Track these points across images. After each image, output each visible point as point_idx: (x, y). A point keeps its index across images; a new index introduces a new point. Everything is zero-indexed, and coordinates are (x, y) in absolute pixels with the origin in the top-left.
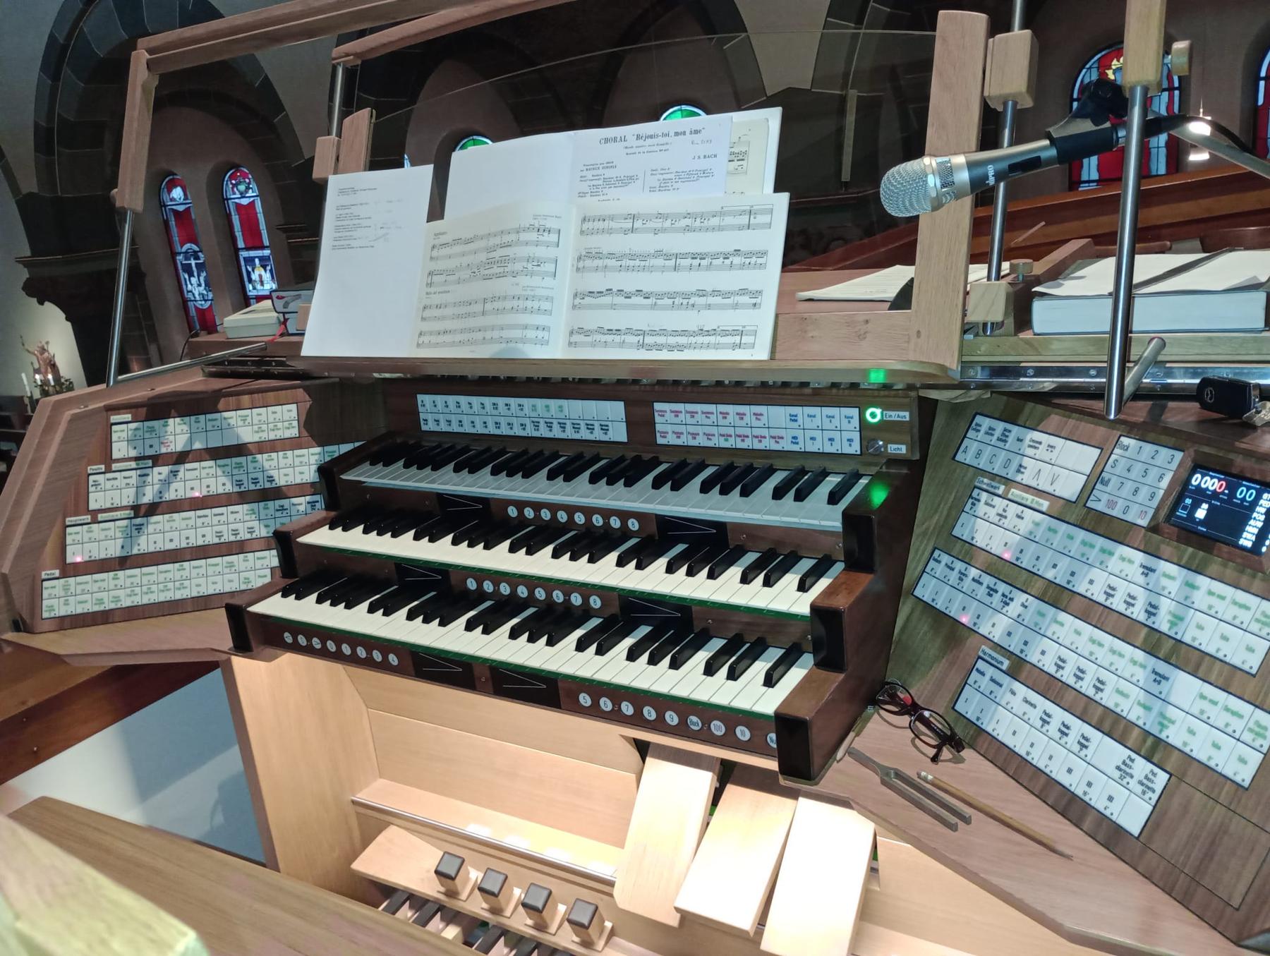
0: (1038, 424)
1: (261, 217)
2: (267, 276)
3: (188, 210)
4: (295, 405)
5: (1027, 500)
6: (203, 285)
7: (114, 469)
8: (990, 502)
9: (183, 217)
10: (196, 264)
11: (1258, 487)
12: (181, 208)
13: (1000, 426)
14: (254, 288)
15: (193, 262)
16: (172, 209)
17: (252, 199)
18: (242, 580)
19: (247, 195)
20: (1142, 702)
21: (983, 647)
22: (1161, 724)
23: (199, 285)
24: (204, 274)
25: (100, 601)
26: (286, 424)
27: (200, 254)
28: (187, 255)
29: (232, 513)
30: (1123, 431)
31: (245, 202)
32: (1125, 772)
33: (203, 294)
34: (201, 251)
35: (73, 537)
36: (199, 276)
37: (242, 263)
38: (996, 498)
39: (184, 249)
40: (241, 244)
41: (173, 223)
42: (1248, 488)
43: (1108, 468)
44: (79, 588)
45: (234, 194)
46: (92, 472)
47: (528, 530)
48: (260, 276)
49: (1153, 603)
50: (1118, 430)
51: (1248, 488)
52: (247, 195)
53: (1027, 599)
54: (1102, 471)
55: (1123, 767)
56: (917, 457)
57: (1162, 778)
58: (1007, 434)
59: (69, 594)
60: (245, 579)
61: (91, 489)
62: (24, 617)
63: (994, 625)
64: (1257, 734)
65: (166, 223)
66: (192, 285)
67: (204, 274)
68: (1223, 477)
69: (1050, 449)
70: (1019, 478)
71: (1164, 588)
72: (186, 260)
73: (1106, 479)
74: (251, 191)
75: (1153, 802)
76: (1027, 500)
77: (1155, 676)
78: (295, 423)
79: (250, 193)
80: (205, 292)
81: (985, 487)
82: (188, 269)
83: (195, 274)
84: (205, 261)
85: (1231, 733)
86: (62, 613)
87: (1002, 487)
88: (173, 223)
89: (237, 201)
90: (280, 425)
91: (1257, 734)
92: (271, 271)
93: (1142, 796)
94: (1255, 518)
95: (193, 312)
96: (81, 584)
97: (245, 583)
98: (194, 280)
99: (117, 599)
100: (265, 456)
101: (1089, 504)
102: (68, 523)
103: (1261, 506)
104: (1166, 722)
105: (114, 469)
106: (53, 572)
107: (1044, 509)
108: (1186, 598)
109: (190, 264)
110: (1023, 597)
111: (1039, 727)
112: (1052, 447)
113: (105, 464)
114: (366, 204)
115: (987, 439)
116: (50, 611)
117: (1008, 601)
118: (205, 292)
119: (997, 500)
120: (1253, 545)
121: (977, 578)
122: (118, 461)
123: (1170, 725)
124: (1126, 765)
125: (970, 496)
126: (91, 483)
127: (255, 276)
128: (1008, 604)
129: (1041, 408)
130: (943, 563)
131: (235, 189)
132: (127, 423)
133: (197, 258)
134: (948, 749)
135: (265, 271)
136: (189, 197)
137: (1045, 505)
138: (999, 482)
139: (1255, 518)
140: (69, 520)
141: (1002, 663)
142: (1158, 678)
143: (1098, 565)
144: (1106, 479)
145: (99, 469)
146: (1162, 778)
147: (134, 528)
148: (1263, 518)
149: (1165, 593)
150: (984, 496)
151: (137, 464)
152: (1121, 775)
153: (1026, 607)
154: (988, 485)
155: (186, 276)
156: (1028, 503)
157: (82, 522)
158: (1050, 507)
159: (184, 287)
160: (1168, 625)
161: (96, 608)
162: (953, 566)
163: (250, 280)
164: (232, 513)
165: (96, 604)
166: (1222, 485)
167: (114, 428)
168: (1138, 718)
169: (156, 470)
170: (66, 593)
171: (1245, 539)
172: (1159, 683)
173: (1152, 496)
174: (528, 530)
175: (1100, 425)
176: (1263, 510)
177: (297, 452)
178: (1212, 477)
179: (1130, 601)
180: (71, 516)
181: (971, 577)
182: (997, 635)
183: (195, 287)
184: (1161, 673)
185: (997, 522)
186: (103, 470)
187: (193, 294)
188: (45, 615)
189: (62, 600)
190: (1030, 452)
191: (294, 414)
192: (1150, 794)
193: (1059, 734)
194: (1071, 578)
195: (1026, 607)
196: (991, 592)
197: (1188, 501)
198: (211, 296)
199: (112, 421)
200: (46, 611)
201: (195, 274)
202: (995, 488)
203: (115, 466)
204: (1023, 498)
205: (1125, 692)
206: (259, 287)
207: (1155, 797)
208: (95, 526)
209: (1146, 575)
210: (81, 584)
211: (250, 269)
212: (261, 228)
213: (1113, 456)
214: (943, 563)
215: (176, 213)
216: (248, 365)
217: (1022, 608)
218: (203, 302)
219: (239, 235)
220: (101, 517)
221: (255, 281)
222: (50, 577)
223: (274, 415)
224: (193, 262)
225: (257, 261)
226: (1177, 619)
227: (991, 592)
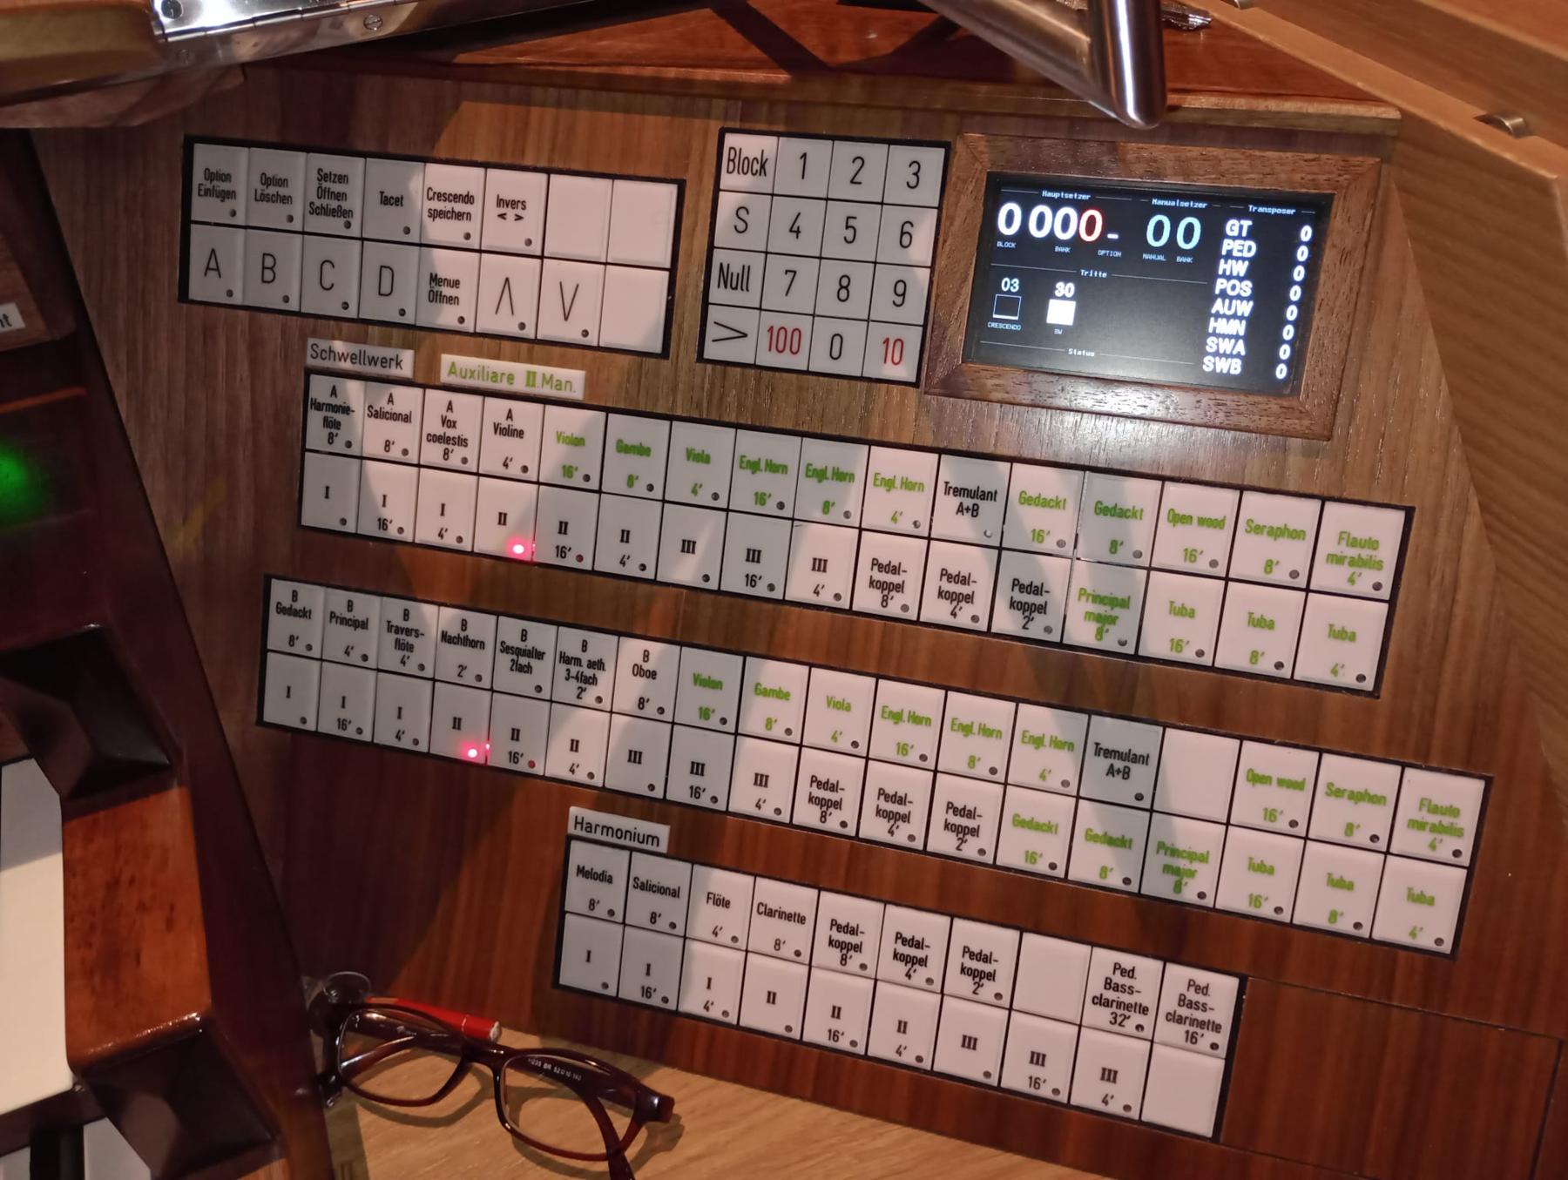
0: (433, 137)
5: (511, 378)
8: (383, 404)
11: (1202, 205)
13: (299, 169)
20: (1099, 831)
21: (574, 811)
22: (1176, 871)
30: (726, 118)
32: (1119, 1004)
38: (400, 392)
42: (1176, 216)
43: (723, 235)
47: (402, 1040)
49: (1025, 581)
50: (708, 115)
51: (1176, 216)
53: (646, 655)
54: (711, 247)
55: (1110, 995)
56: (69, 325)
57: (1222, 990)
58: (337, 188)
63: (574, 746)
64: (1436, 829)
68: (1085, 197)
69: (511, 213)
70: (447, 317)
71: (1039, 535)
73: (736, 269)
75: (1222, 1051)
76: (511, 378)
77: (1109, 761)
81: (346, 365)
85: (1287, 829)
87: (407, 356)
91: (1436, 829)
93: (1189, 1045)
94: (1223, 295)
101: (712, 351)
103: (1229, 255)
104: (1182, 863)
107: (578, 394)
108: (1114, 546)
110: (633, 649)
111: (836, 964)
112: (513, 204)
114: (220, 276)
115: (272, 214)
117: (589, 672)
119: (406, 399)
120: (1244, 367)
121: (454, 631)
123: (1195, 866)
124: (1116, 988)
125: (307, 403)
128: (593, 681)
129: (414, 89)
130: (318, 615)
134: (363, 1081)
137: (573, 380)
138: (386, 343)
139: (1223, 295)
141: (654, 839)
142: (1119, 764)
143: (817, 515)
144: (736, 269)
146: (1222, 990)
148: (1246, 288)
149: (1049, 545)
150: (354, 392)
152: (1115, 1016)
153: (652, 675)
154: (353, 358)
156: (519, 386)
158: (590, 384)
160: (1093, 627)
162: (358, 614)
166: (1092, 220)
168: (1104, 871)
171: (1217, 354)
172: (1126, 774)
173: (901, 293)
174: (402, 1040)
175: (643, 112)
176: (1241, 268)
178: (1055, 205)
179: (956, 588)
181: (433, 633)
182: (590, 766)
184: (1123, 749)
185: (441, 462)
190: (440, 231)
192: (1209, 1037)
193: (901, 968)
194: (563, 541)
195: (652, 675)
196: (523, 661)
197: (1010, 285)
202: (385, 362)
204: (559, 385)
205: (1042, 819)
207: (1222, 1039)
209: (974, 511)
213: (724, 197)
214: (318, 615)
217: (641, 682)
226: (1108, 606)
227: (523, 661)
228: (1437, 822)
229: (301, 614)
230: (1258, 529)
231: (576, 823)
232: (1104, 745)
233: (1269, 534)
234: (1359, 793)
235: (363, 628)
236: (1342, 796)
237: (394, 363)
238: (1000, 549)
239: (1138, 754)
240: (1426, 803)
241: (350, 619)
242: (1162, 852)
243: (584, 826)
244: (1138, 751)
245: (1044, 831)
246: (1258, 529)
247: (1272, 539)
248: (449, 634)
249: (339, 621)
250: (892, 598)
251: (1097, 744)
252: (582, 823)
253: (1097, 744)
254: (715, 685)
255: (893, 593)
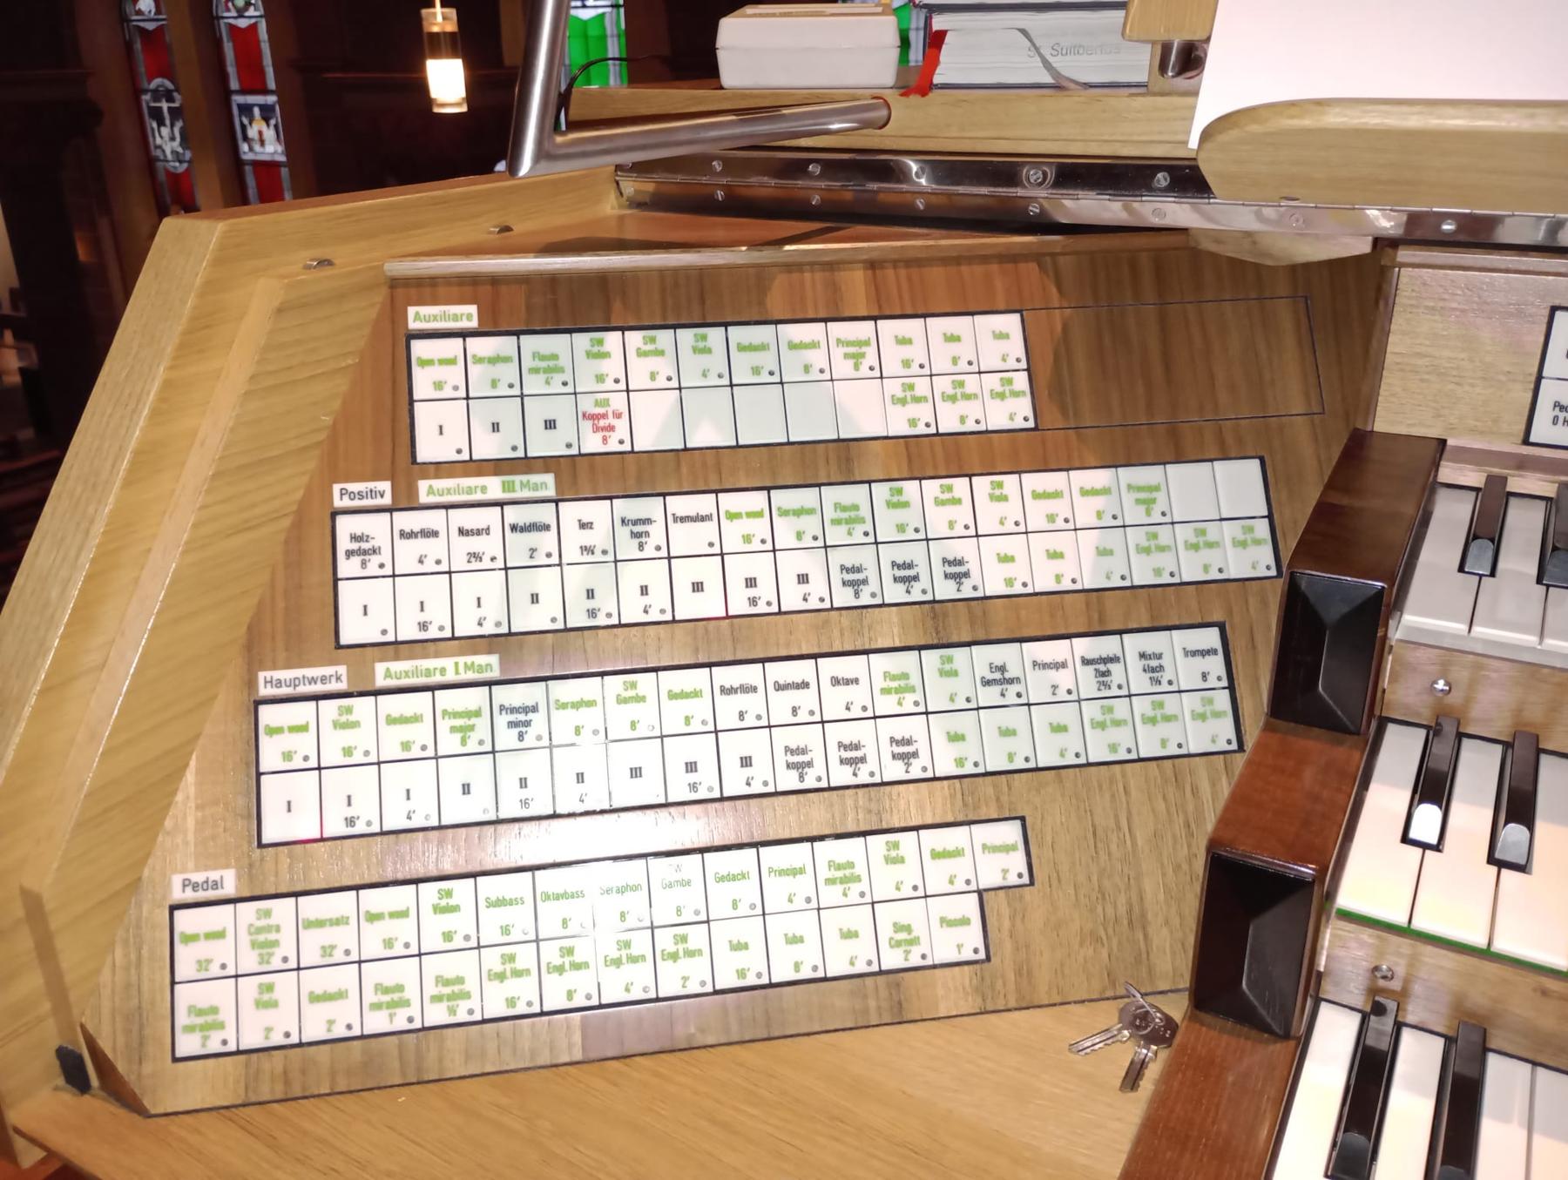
1: (266, 48)
2: (269, 134)
3: (160, 29)
4: (1016, 318)
6: (178, 139)
7: (424, 498)
9: (153, 39)
10: (169, 108)
12: (150, 26)
14: (251, 149)
15: (165, 105)
16: (138, 27)
17: (253, 21)
18: (886, 932)
19: (247, 14)
23: (173, 139)
24: (179, 124)
25: (393, 996)
26: (992, 381)
27: (176, 94)
28: (157, 95)
29: (836, 681)
31: (243, 23)
33: (177, 153)
34: (177, 90)
35: (287, 741)
36: (172, 125)
37: (235, 111)
39: (153, 85)
40: (234, 84)
41: (138, 46)
44: (312, 943)
45: (228, 10)
46: (346, 503)
48: (260, 133)
52: (247, 14)
59: (276, 963)
60: (898, 928)
61: (346, 567)
62: (105, 1045)
65: (129, 46)
66: (161, 137)
67: (179, 124)
72: (155, 101)
74: (252, 8)
78: (1021, 381)
79: (251, 12)
80: (180, 150)
82: (157, 114)
83: (168, 122)
84: (181, 105)
86: (252, 1039)
88: (138, 46)
89: (231, 21)
90: (972, 383)
92: (276, 127)
95: (162, 177)
96: (320, 924)
97: (898, 944)
98: (165, 131)
99: (452, 989)
100: (932, 487)
102: (265, 691)
105: (424, 498)
106: (214, 875)
109: (160, 109)
113: (393, 478)
116: (205, 1028)
118: (180, 150)
122: (441, 469)
126: (344, 544)
127: (252, 132)
131: (230, 4)
132: (464, 334)
133: (170, 99)
135: (268, 125)
136: (163, 10)
140: (269, 681)
145: (372, 493)
147: (502, 720)
151: (507, 487)
155: (155, 125)
157: (318, 688)
159: (151, 139)
161: (377, 1023)
163: (246, 138)
164: (836, 681)
165: (376, 1007)
167: (419, 348)
169: (572, 511)
170: (264, 960)
177: (1034, 481)
180: (275, 667)
183: (167, 141)
186: (387, 500)
187: (164, 151)
188: (188, 1045)
189: (249, 986)
191: (1016, 347)
198: (188, 155)
199: (414, 325)
200: (189, 1029)
201: (168, 122)
203: (426, 490)
206: (257, 148)
208: (363, 705)
210: (320, 924)
211: (246, 121)
212: (265, 63)
215: (143, 31)
216: (810, 176)
218: (177, 164)
219: (231, 70)
220: (384, 672)
221: (252, 140)
222: (201, 895)
223: (954, 348)
224: (165, 105)
225: (256, 111)
228: (847, 517)
229: (739, 877)
230: (564, 706)
231: (266, 682)
232: (679, 514)
233: (572, 707)
234: (578, 702)
235: (1064, 668)
236: (567, 708)
237: (333, 679)
238: (716, 732)
239: (704, 514)
240: (379, 987)
241: (788, 869)
242: (447, 717)
243: (274, 683)
244: (703, 513)
245: (692, 697)
246: (564, 706)
247: (575, 710)
248: (465, 528)
249: (509, 711)
250: (806, 773)
251: (674, 515)
252: (271, 682)
253: (674, 515)
254: (957, 339)
255: (806, 770)
